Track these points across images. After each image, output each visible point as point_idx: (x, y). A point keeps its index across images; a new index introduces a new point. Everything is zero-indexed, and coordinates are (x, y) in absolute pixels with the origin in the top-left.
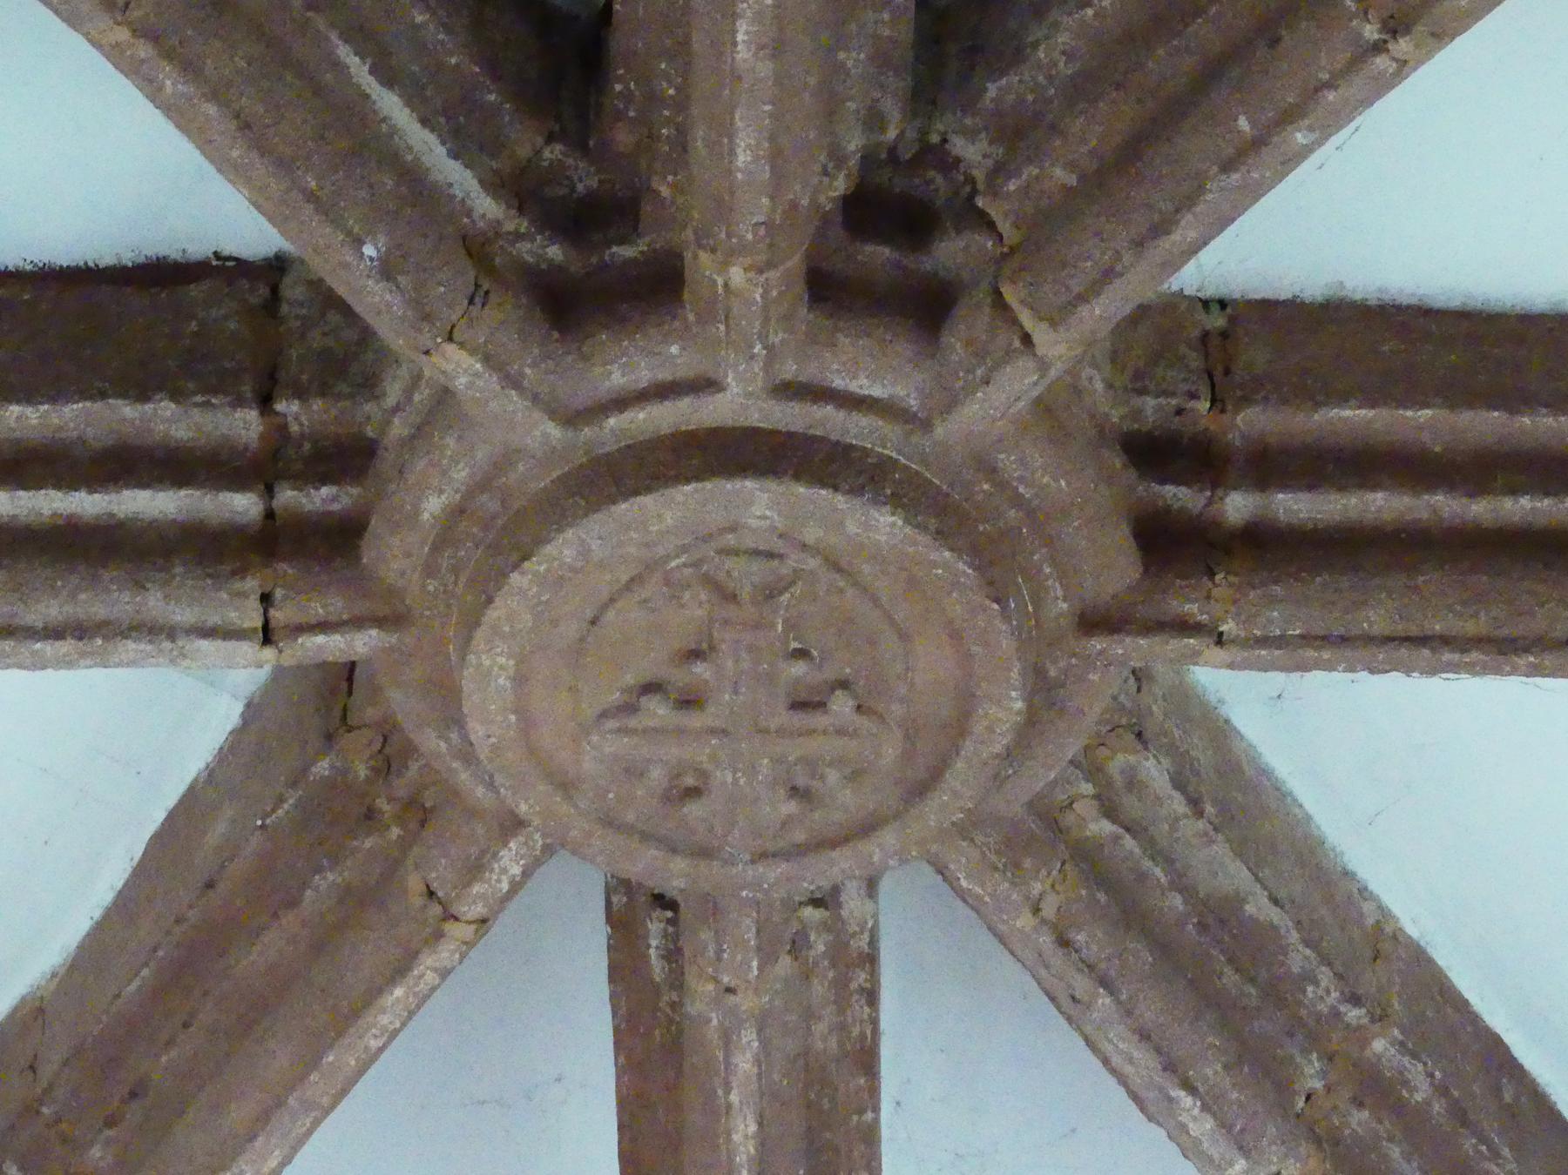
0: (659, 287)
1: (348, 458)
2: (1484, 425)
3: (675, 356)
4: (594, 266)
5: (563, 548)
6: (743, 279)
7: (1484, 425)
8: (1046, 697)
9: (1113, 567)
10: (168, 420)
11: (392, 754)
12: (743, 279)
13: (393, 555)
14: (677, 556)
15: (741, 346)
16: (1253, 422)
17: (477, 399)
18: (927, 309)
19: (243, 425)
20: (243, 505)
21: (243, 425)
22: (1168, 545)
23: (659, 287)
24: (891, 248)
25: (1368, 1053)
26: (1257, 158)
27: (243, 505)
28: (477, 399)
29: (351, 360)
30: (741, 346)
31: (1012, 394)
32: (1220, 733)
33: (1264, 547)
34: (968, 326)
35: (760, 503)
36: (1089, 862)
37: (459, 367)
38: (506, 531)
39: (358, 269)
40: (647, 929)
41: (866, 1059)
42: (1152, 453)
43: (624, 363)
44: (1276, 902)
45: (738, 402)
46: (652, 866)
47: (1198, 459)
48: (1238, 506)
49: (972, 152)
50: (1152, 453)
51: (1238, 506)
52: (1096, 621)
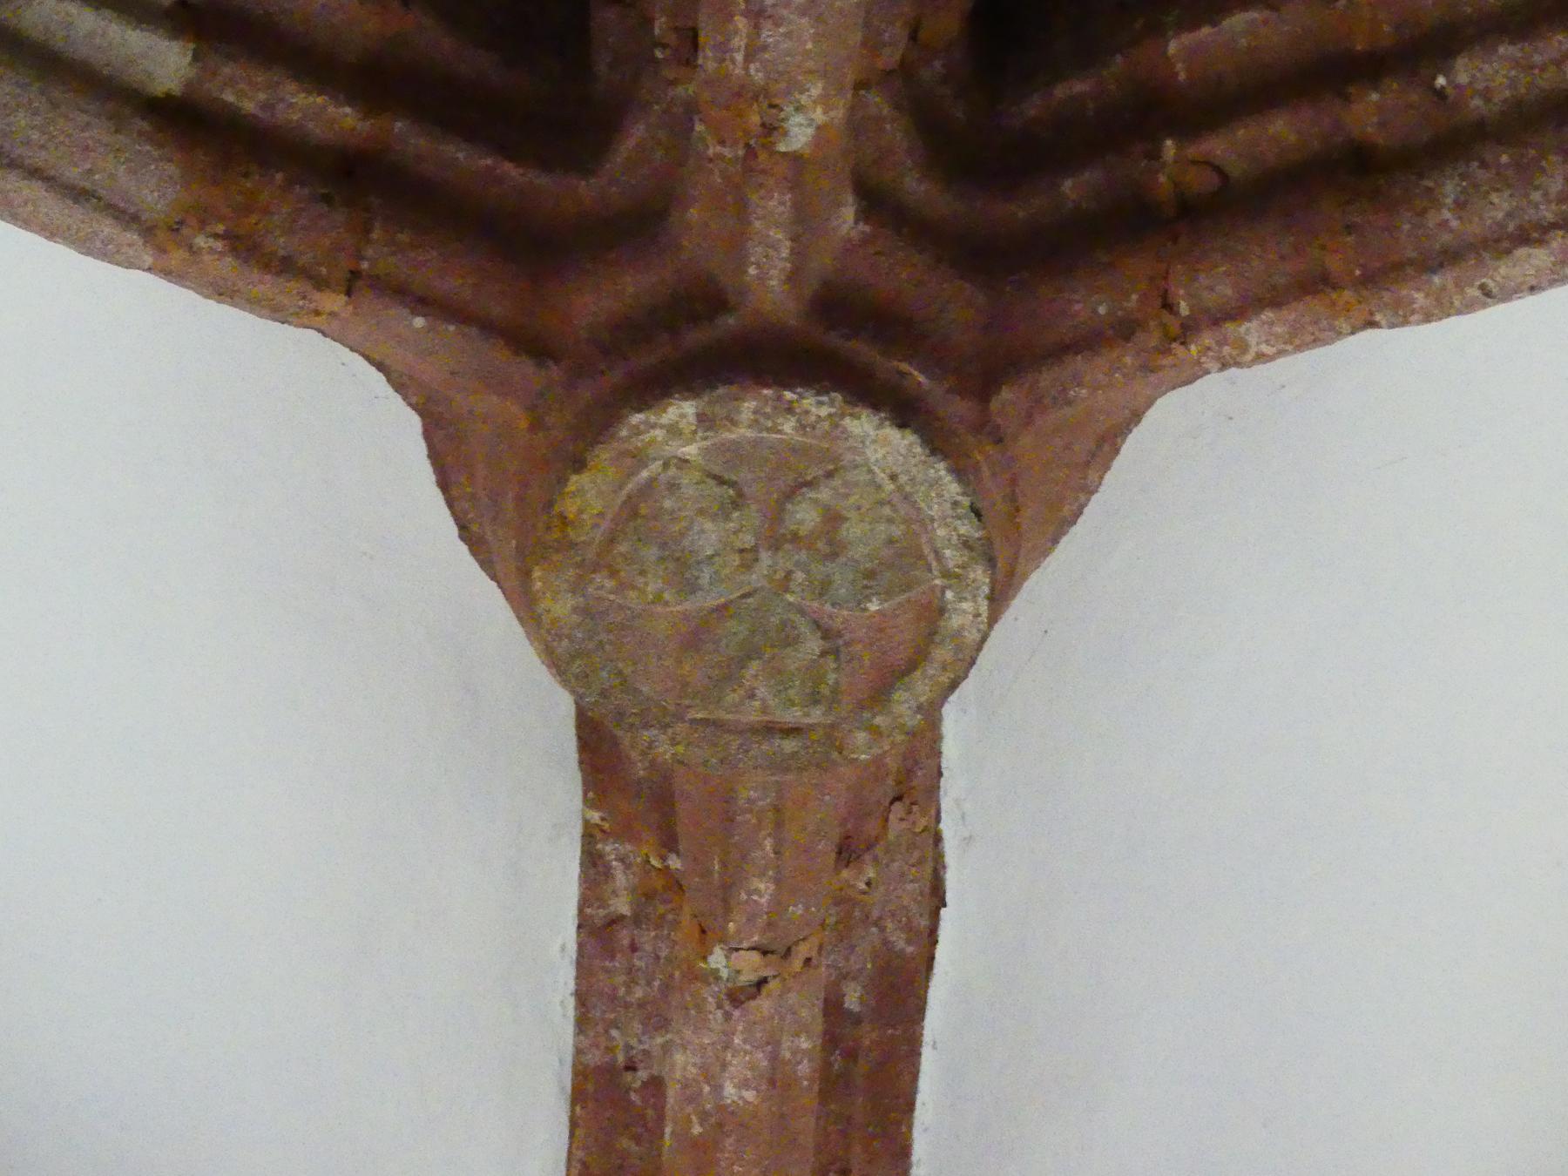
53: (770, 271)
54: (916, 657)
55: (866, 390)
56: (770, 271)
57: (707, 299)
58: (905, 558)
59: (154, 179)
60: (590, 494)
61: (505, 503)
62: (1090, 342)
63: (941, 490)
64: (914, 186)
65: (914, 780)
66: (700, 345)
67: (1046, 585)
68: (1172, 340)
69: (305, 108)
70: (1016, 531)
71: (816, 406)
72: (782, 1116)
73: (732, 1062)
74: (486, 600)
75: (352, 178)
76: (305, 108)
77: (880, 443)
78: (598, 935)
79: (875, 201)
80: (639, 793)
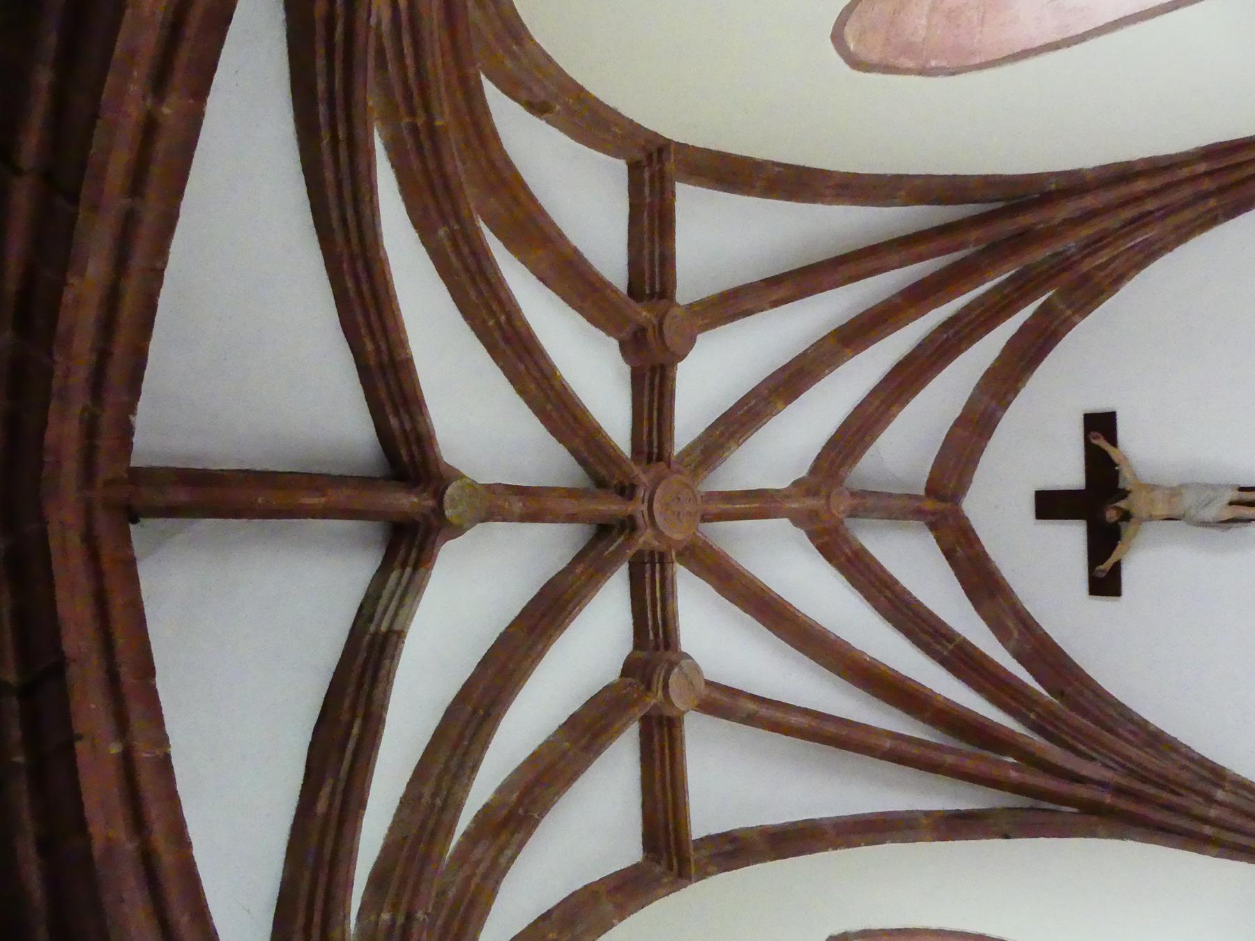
0: (631, 518)
1: (652, 553)
2: (645, 422)
3: (639, 516)
4: (629, 526)
5: (662, 528)
6: (630, 508)
7: (645, 422)
8: (679, 472)
9: (662, 465)
10: (647, 575)
11: (686, 548)
12: (630, 508)
13: (664, 548)
14: (478, 885)
15: (638, 508)
16: (646, 448)
17: (645, 539)
18: (633, 487)
19: (648, 566)
20: (658, 566)
21: (648, 566)
22: (660, 458)
23: (631, 518)
24: (626, 491)
25: (849, 523)
26: (615, 448)
27: (658, 566)
28: (645, 539)
29: (640, 553)
30: (638, 508)
31: (642, 476)
32: (681, 453)
33: (660, 446)
34: (635, 482)
35: (656, 506)
36: (696, 468)
37: (641, 541)
38: (659, 534)
39: (630, 553)
40: (705, 518)
41: (721, 493)
42: (650, 460)
43: (640, 522)
44: (649, 688)
45: (644, 508)
46: (698, 517)
47: (650, 454)
48: (655, 450)
49: (615, 482)
50: (650, 460)
51: (655, 450)
52: (669, 465)
53: (431, 503)
54: (473, 484)
55: (443, 492)
56: (431, 503)
57: (433, 510)
58: (462, 487)
59: (422, 570)
60: (455, 521)
61: (457, 531)
62: (1135, 475)
63: (454, 484)
64: (421, 487)
65: (488, 487)
66: (439, 510)
67: (464, 471)
68: (438, 460)
69: (413, 555)
70: (457, 475)
71: (446, 497)
72: (982, 25)
73: (517, 506)
74: (468, 533)
75: (421, 549)
76: (413, 555)
77: (449, 491)
78: (504, 520)
79: (423, 491)
80: (492, 515)
